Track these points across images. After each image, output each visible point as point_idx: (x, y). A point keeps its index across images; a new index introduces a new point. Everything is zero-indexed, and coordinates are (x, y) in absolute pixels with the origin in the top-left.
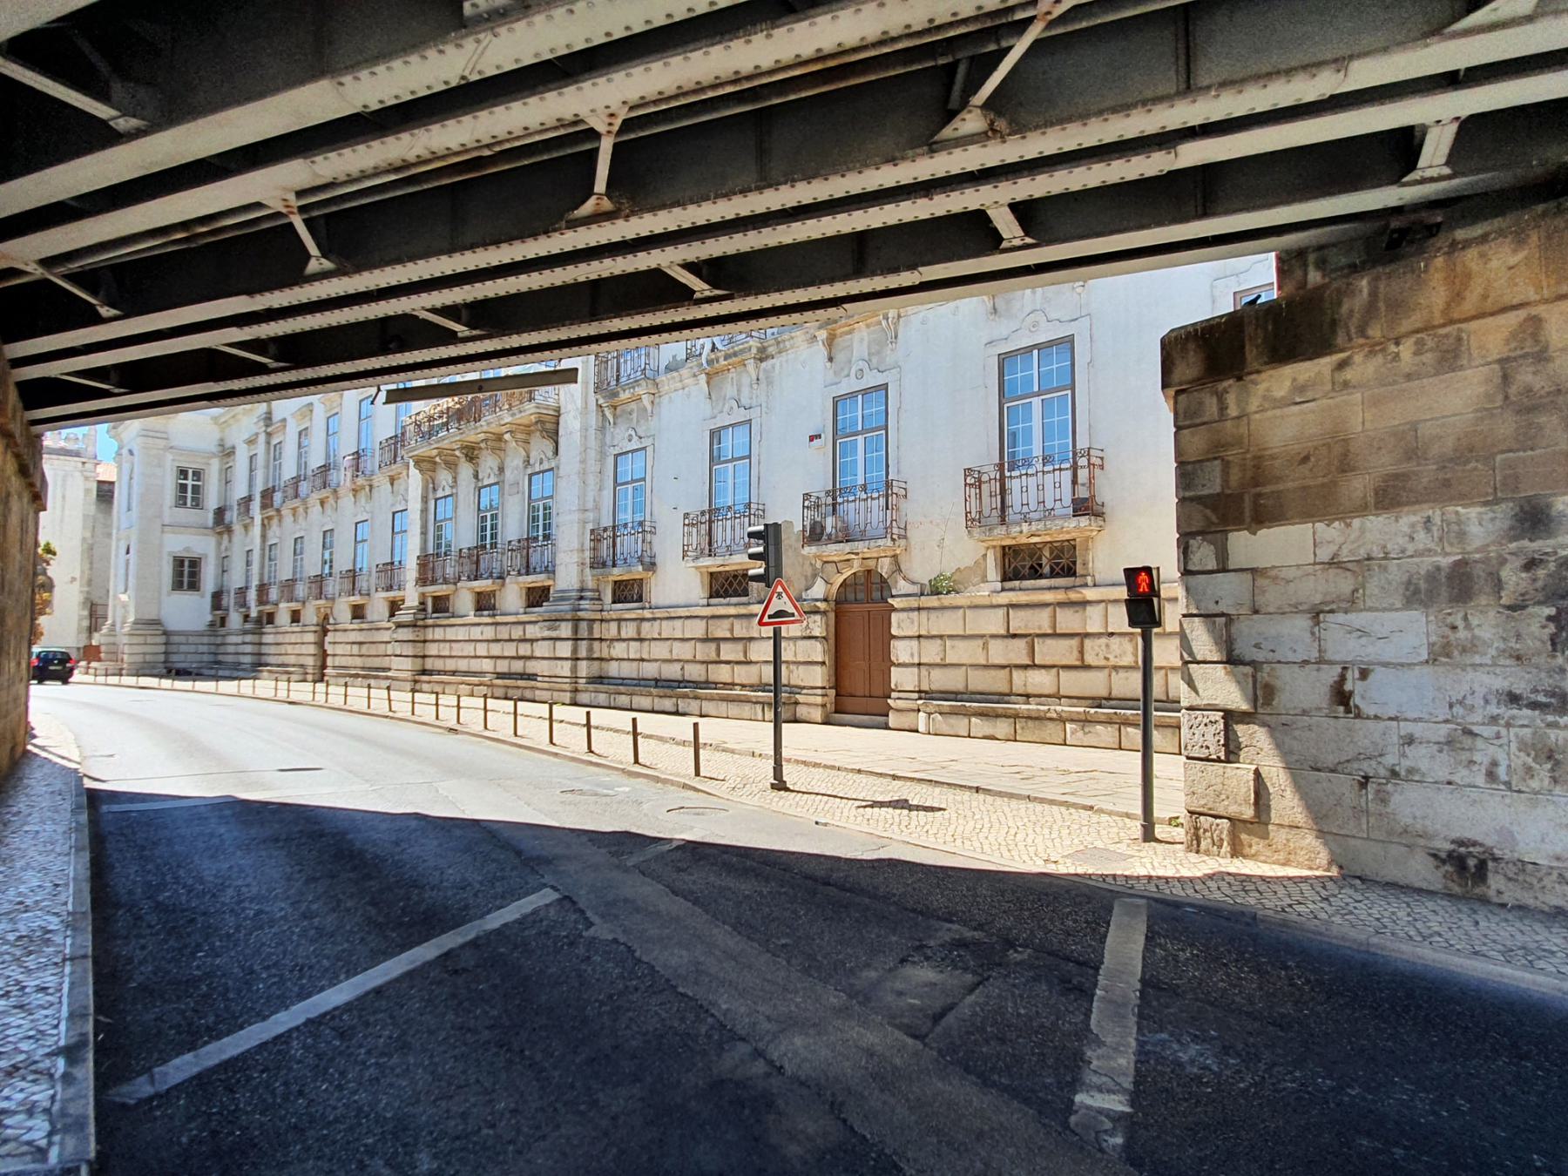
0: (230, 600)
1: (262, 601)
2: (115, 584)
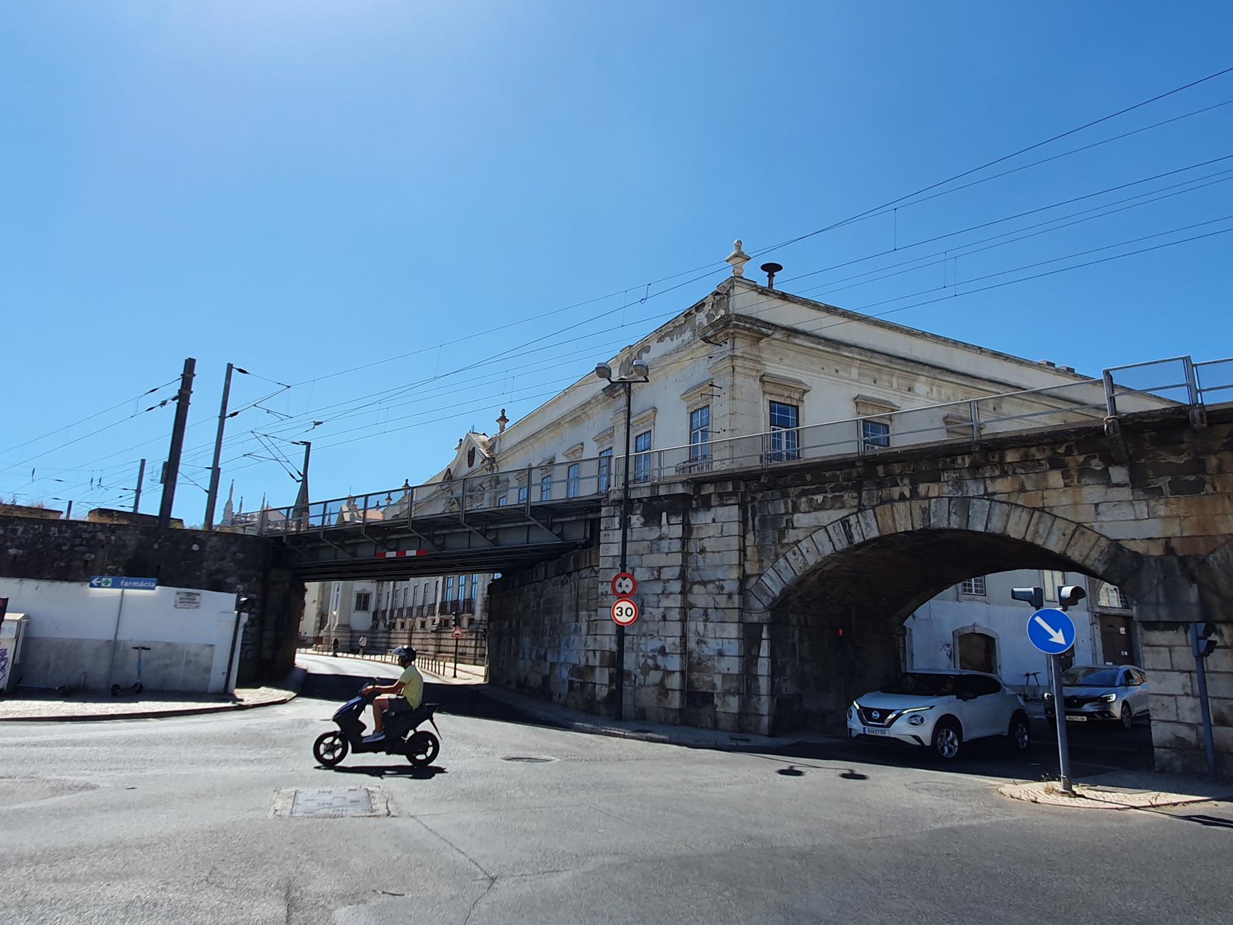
0: (379, 616)
1: (391, 617)
2: (332, 605)
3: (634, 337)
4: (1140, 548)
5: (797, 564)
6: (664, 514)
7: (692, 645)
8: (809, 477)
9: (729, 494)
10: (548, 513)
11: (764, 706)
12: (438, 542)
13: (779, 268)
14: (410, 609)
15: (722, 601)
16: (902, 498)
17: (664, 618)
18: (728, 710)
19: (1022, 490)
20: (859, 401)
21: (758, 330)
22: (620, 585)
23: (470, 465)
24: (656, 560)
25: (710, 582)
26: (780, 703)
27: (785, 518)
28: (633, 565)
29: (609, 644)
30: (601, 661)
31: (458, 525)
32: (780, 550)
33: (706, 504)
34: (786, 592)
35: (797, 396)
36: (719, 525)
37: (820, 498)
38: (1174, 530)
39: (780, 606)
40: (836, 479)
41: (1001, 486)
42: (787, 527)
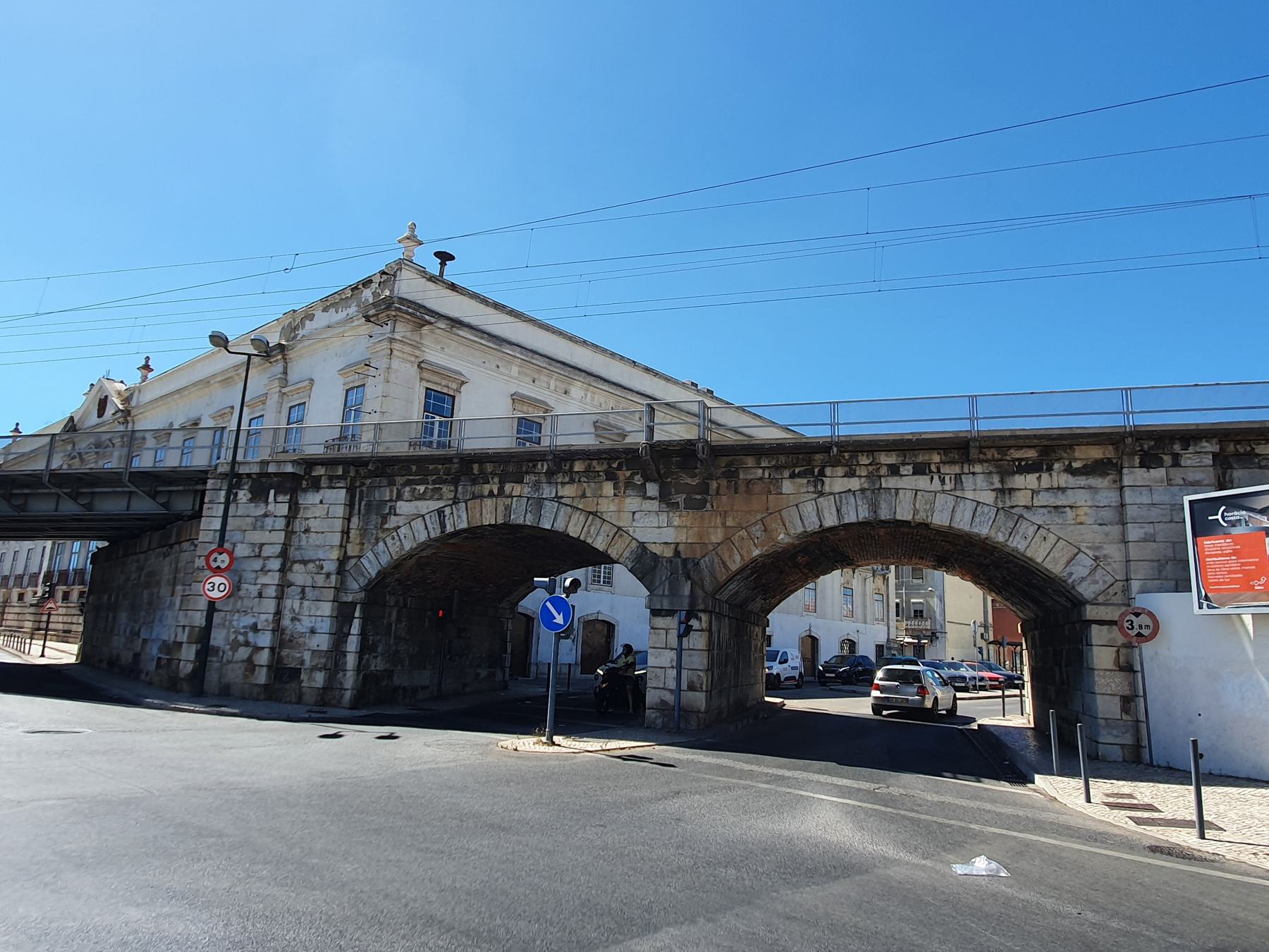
3: (299, 302)
4: (657, 550)
5: (394, 549)
6: (272, 492)
7: (286, 622)
8: (414, 468)
9: (339, 477)
10: (154, 481)
11: (349, 680)
12: (18, 502)
13: (452, 258)
14: (21, 577)
15: (320, 580)
16: (491, 494)
17: (260, 595)
18: (314, 685)
19: (583, 496)
20: (517, 399)
21: (421, 315)
22: (215, 560)
23: (100, 415)
24: (258, 537)
25: (310, 561)
26: (367, 678)
27: (389, 504)
28: (234, 540)
29: (199, 619)
30: (189, 637)
31: (43, 486)
32: (381, 535)
33: (316, 485)
34: (383, 574)
35: (454, 386)
36: (326, 508)
37: (422, 488)
38: (682, 538)
39: (377, 589)
40: (436, 472)
41: (568, 491)
42: (389, 514)
